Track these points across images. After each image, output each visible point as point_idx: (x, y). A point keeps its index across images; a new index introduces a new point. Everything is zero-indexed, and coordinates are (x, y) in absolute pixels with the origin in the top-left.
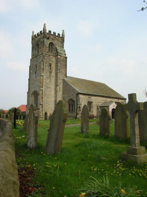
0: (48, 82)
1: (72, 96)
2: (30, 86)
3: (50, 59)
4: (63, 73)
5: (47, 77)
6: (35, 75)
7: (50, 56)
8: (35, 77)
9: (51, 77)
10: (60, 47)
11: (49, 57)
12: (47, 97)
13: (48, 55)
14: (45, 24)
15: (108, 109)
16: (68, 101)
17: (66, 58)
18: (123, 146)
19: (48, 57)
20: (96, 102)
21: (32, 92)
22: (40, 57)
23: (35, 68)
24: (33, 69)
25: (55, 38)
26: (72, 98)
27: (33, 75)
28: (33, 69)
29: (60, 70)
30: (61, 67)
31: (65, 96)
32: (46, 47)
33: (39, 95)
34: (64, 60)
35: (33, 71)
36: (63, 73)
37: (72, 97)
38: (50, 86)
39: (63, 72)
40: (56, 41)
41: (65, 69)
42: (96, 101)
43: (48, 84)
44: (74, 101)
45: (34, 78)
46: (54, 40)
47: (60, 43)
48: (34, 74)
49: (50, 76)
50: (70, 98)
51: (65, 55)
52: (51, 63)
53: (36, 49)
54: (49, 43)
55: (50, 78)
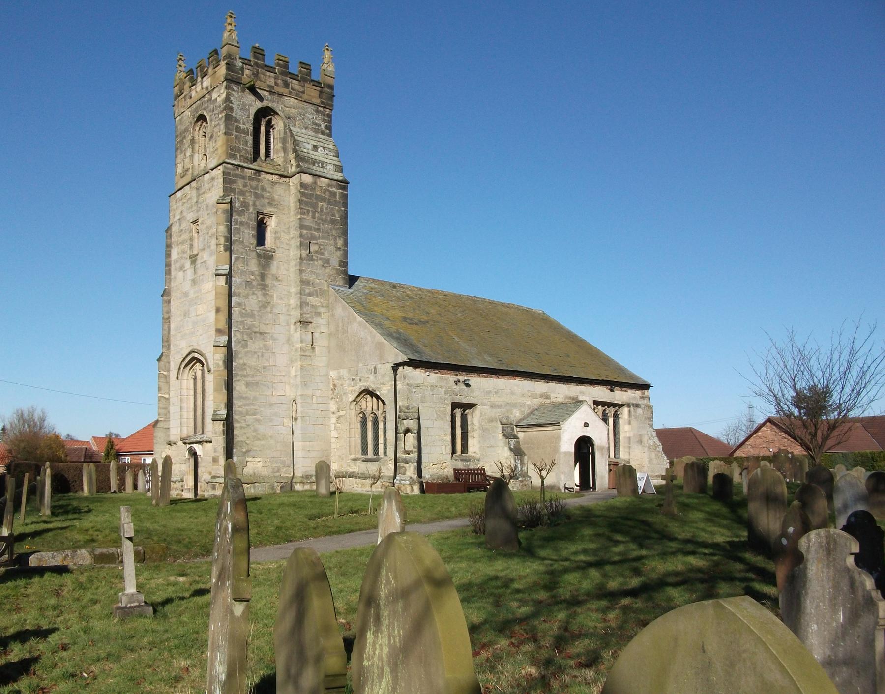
0: (256, 308)
2: (172, 326)
3: (263, 189)
4: (327, 262)
5: (248, 283)
6: (190, 273)
8: (194, 282)
9: (269, 281)
10: (311, 133)
11: (254, 183)
12: (249, 379)
13: (248, 173)
15: (558, 438)
19: (251, 179)
20: (493, 406)
22: (213, 179)
25: (286, 85)
27: (181, 274)
29: (314, 248)
30: (318, 230)
32: (238, 129)
34: (333, 194)
36: (327, 262)
38: (263, 328)
39: (326, 255)
40: (292, 101)
42: (495, 399)
43: (252, 315)
46: (281, 95)
47: (310, 109)
49: (263, 276)
54: (253, 111)
55: (264, 287)
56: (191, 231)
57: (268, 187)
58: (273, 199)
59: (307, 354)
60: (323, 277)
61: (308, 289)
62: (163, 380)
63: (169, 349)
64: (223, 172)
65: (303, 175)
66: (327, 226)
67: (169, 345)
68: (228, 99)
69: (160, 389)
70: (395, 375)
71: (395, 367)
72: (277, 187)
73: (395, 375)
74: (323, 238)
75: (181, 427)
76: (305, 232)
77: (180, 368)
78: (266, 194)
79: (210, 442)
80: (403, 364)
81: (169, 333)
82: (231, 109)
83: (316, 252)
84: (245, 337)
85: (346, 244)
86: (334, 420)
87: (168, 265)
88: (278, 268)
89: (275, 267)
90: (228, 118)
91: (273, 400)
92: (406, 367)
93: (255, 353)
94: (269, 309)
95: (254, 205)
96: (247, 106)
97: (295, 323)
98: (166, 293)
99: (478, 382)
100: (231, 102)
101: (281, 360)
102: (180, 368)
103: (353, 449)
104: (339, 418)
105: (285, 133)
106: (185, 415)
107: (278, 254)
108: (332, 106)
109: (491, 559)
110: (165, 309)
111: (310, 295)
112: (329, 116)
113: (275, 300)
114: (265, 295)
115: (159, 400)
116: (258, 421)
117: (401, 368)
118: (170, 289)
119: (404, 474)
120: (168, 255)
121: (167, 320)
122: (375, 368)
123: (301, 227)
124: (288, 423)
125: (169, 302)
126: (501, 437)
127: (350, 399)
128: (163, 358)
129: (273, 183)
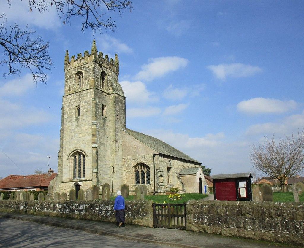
1: (143, 159)
2: (64, 141)
3: (104, 97)
6: (75, 123)
7: (104, 94)
8: (77, 126)
9: (105, 127)
11: (101, 95)
14: (31, 30)
15: (195, 178)
16: (134, 167)
17: (124, 98)
18: (59, 228)
21: (68, 152)
22: (88, 93)
23: (75, 112)
24: (70, 113)
26: (143, 162)
27: (70, 123)
28: (70, 113)
30: (119, 112)
31: (128, 159)
32: (97, 78)
33: (87, 156)
34: (122, 101)
35: (71, 116)
36: (121, 122)
37: (143, 161)
38: (104, 142)
41: (124, 116)
43: (101, 138)
44: (148, 166)
45: (73, 127)
48: (74, 120)
49: (104, 125)
50: (139, 161)
51: (123, 93)
52: (105, 104)
53: (75, 79)
55: (104, 129)
56: (75, 109)
57: (105, 97)
58: (106, 101)
59: (117, 151)
60: (119, 126)
61: (117, 130)
62: (60, 160)
63: (62, 148)
64: (94, 91)
65: (116, 94)
66: (121, 111)
67: (63, 147)
68: (94, 68)
69: (59, 163)
70: (154, 158)
71: (154, 156)
72: (107, 97)
73: (154, 158)
74: (120, 115)
75: (69, 176)
76: (116, 112)
77: (69, 155)
78: (104, 99)
79: (91, 180)
80: (157, 155)
81: (63, 143)
82: (95, 71)
83: (119, 119)
84: (100, 145)
85: (125, 117)
86: (125, 173)
87: (63, 120)
88: (107, 123)
89: (107, 123)
90: (94, 73)
91: (107, 166)
92: (158, 156)
93: (102, 150)
94: (105, 136)
95: (102, 102)
96: (99, 71)
97: (113, 141)
98: (62, 130)
99: (173, 161)
100: (95, 68)
101: (109, 153)
102: (69, 155)
103: (133, 183)
104: (127, 172)
105: (108, 80)
106: (71, 172)
107: (108, 118)
108: (118, 73)
109: (56, 227)
110: (62, 135)
111: (118, 132)
112: (118, 76)
113: (107, 133)
114: (104, 131)
115: (58, 167)
116: (103, 173)
117: (156, 156)
118: (63, 128)
119: (161, 189)
120: (63, 116)
121: (62, 138)
122: (144, 156)
123: (115, 110)
124: (111, 174)
125: (63, 132)
126: (176, 178)
127: (133, 166)
128: (60, 152)
129: (106, 96)
